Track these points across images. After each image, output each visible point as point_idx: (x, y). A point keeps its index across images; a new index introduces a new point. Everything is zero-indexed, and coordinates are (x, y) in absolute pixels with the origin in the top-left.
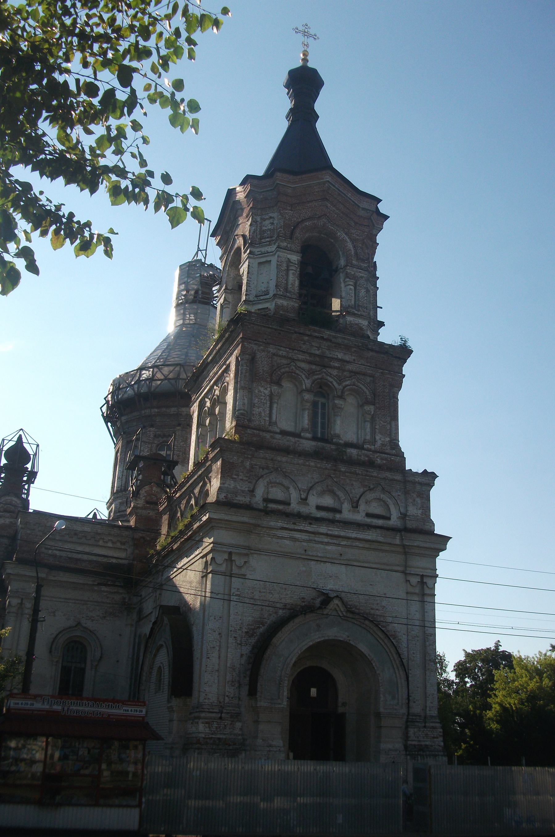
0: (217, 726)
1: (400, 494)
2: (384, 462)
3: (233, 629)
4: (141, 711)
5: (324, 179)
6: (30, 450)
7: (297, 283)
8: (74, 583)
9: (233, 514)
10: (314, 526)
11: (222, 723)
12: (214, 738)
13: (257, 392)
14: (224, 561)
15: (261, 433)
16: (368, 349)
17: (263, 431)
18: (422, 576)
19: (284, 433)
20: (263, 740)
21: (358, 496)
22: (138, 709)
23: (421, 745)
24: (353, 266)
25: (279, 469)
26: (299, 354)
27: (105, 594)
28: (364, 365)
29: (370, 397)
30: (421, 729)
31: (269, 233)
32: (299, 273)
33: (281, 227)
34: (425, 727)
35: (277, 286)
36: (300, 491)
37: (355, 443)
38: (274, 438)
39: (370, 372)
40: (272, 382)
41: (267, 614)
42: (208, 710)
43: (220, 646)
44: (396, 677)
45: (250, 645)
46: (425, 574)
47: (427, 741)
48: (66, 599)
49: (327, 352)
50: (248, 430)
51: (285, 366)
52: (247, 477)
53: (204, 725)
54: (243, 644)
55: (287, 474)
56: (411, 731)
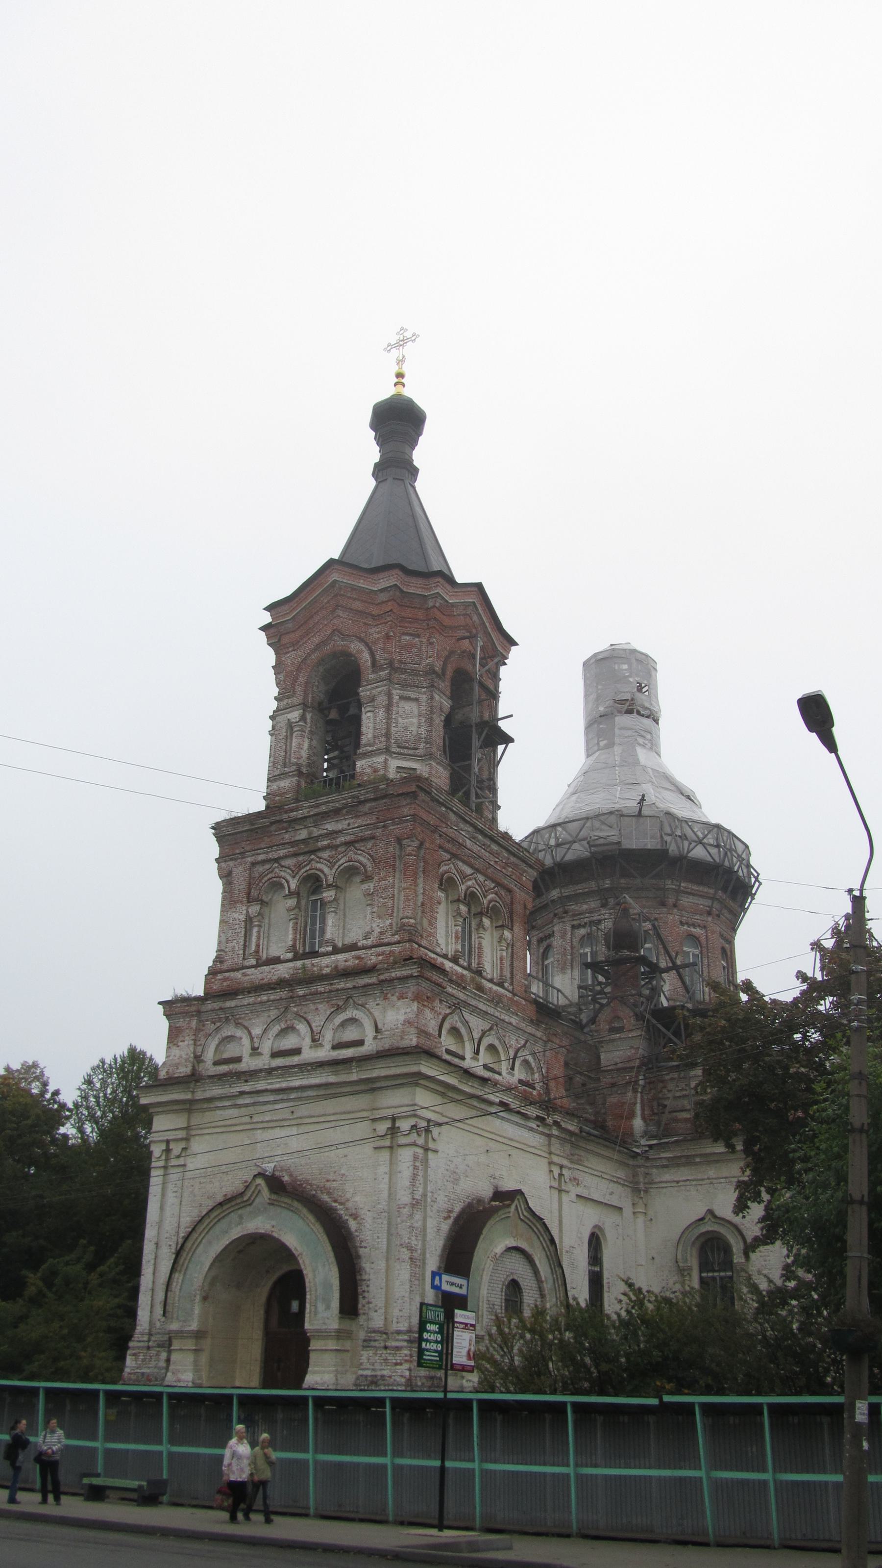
2: (380, 958)
15: (232, 974)
16: (361, 803)
21: (322, 1023)
23: (376, 1376)
26: (280, 850)
34: (386, 1348)
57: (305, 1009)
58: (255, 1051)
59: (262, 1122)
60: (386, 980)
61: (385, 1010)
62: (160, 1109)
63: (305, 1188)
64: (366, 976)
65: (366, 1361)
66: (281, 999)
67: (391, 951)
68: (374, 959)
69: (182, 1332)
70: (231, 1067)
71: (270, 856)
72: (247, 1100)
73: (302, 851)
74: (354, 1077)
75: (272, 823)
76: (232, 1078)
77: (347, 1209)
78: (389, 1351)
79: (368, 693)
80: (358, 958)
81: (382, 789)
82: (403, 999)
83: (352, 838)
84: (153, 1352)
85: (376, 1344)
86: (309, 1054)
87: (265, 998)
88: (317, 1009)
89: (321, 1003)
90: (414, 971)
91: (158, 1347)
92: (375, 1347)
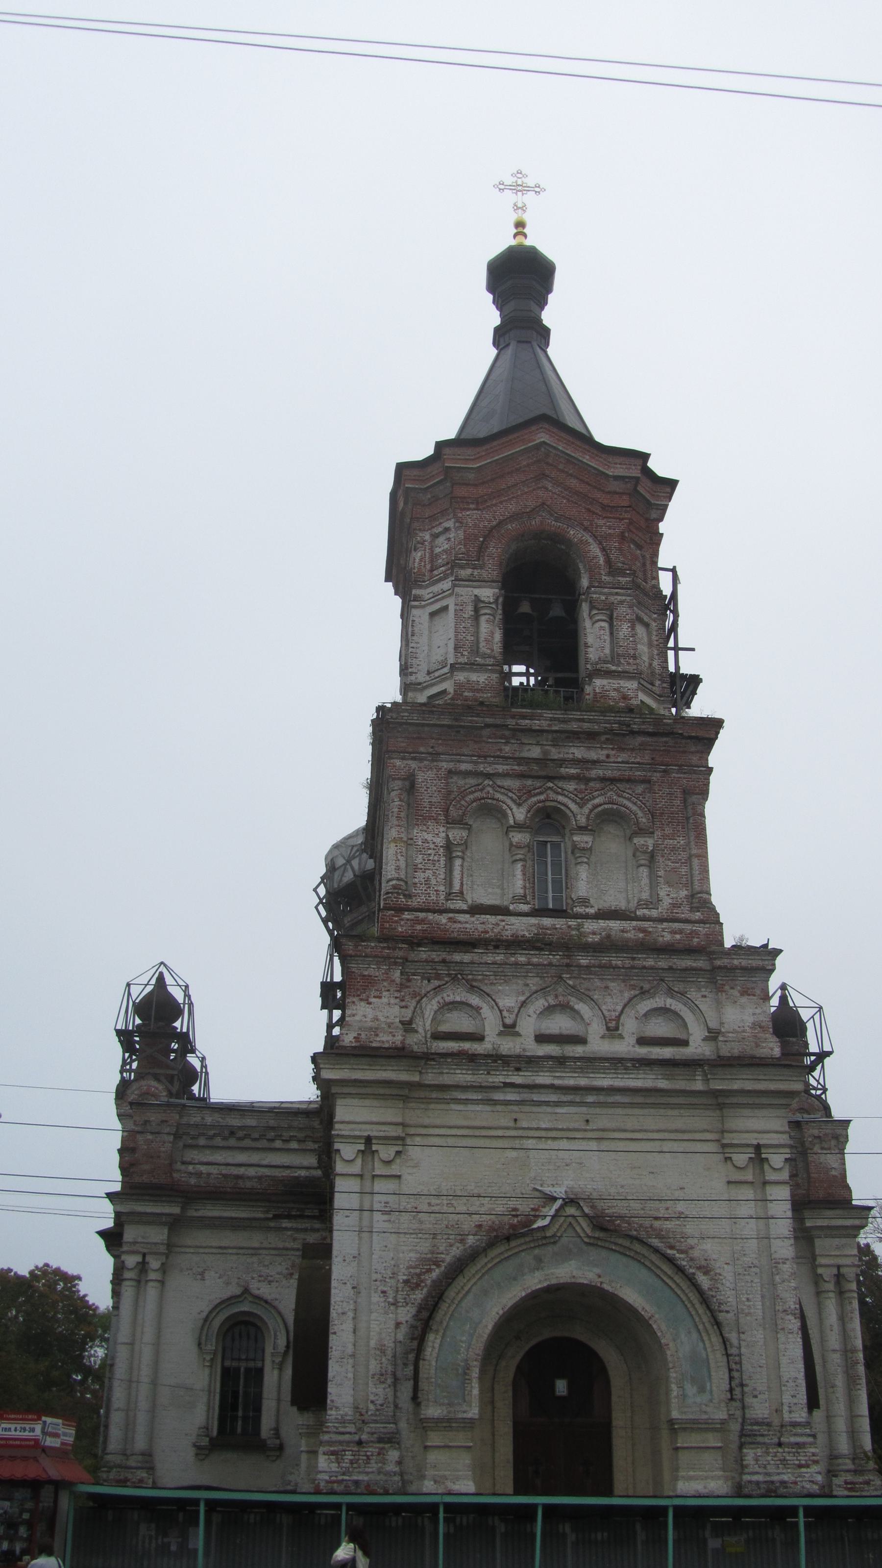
0: (352, 1457)
1: (706, 993)
2: (678, 937)
3: (379, 1277)
4: (33, 1430)
5: (535, 440)
6: (178, 995)
7: (498, 636)
8: (232, 1218)
9: (365, 1067)
10: (526, 1074)
11: (362, 1453)
13: (420, 843)
14: (358, 1154)
15: (430, 916)
16: (633, 733)
17: (434, 911)
18: (758, 1148)
19: (477, 910)
20: (435, 1482)
21: (619, 1008)
22: (27, 1427)
23: (772, 1482)
24: (602, 585)
25: (459, 976)
26: (498, 764)
27: (289, 1233)
28: (627, 763)
29: (644, 820)
31: (444, 557)
32: (501, 617)
33: (460, 543)
34: (780, 1444)
35: (456, 648)
36: (501, 1011)
37: (623, 908)
38: (455, 922)
39: (639, 773)
40: (451, 822)
41: (444, 1245)
42: (335, 1430)
43: (355, 1310)
45: (412, 1304)
46: (761, 1142)
47: (784, 1473)
48: (220, 1248)
49: (553, 750)
50: (406, 913)
51: (473, 789)
52: (396, 998)
53: (327, 1457)
54: (400, 1304)
55: (475, 984)
56: (750, 1455)
58: (509, 1029)
59: (538, 1129)
60: (725, 967)
61: (719, 1005)
62: (346, 1090)
63: (619, 1225)
65: (752, 1462)
67: (692, 932)
68: (667, 937)
69: (449, 1420)
70: (466, 1046)
71: (481, 768)
73: (534, 773)
75: (487, 726)
77: (692, 1259)
79: (603, 598)
81: (667, 724)
82: (749, 995)
83: (616, 774)
84: (372, 1450)
86: (598, 1045)
87: (522, 959)
88: (607, 987)
89: (613, 980)
92: (764, 1443)
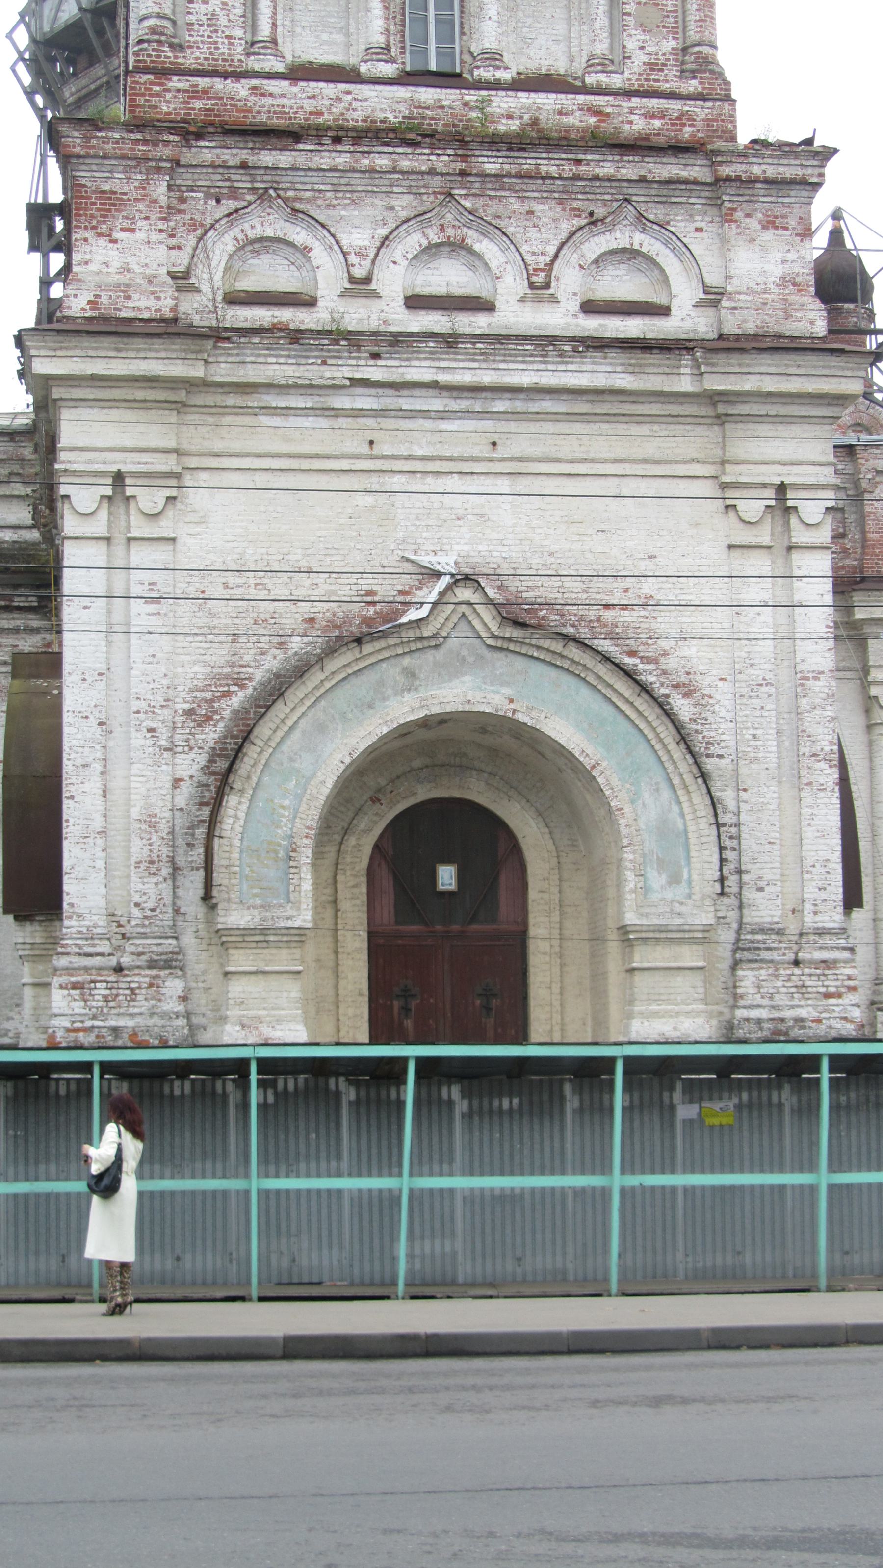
0: (108, 992)
1: (702, 225)
2: (657, 123)
3: (143, 705)
12: (98, 1027)
14: (100, 502)
15: (218, 84)
17: (225, 76)
20: (243, 1026)
21: (552, 250)
23: (782, 1020)
30: (782, 972)
34: (796, 963)
36: (345, 254)
41: (252, 652)
42: (77, 950)
44: (682, 815)
50: (175, 78)
53: (66, 992)
55: (298, 206)
57: (495, 207)
59: (409, 457)
64: (672, 160)
66: (432, 172)
70: (285, 315)
72: (365, 401)
74: (685, 384)
76: (336, 342)
77: (665, 673)
78: (807, 971)
80: (596, 112)
82: (777, 228)
85: (775, 956)
87: (383, 162)
90: (810, 171)
91: (150, 967)
